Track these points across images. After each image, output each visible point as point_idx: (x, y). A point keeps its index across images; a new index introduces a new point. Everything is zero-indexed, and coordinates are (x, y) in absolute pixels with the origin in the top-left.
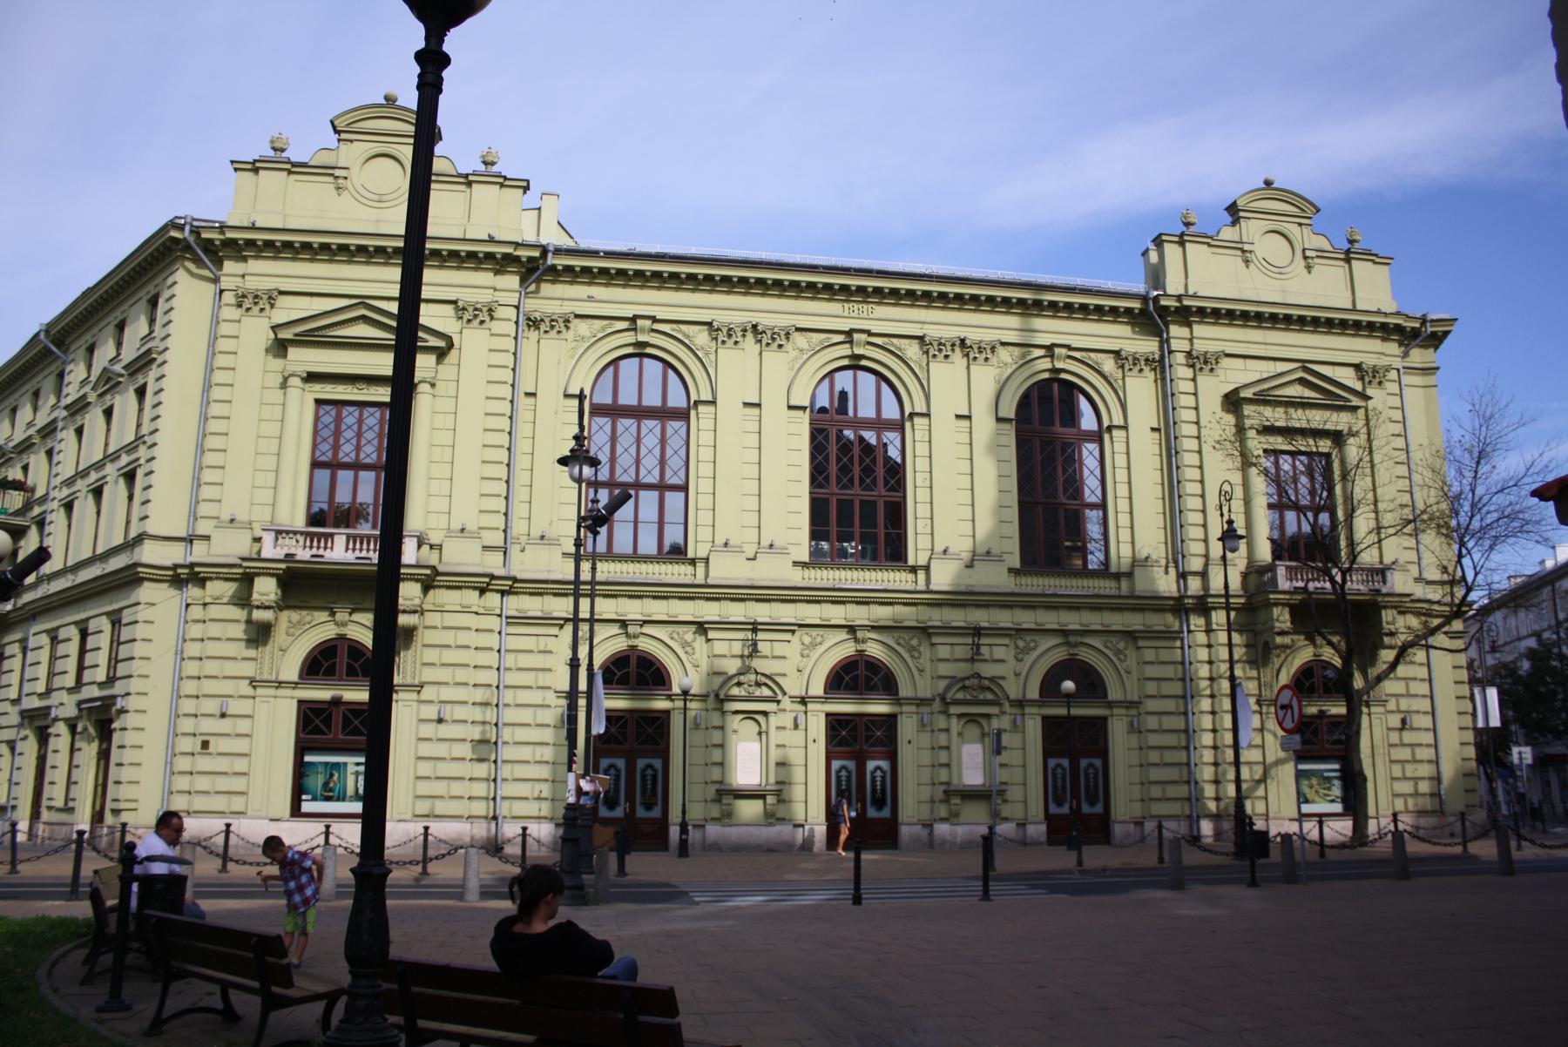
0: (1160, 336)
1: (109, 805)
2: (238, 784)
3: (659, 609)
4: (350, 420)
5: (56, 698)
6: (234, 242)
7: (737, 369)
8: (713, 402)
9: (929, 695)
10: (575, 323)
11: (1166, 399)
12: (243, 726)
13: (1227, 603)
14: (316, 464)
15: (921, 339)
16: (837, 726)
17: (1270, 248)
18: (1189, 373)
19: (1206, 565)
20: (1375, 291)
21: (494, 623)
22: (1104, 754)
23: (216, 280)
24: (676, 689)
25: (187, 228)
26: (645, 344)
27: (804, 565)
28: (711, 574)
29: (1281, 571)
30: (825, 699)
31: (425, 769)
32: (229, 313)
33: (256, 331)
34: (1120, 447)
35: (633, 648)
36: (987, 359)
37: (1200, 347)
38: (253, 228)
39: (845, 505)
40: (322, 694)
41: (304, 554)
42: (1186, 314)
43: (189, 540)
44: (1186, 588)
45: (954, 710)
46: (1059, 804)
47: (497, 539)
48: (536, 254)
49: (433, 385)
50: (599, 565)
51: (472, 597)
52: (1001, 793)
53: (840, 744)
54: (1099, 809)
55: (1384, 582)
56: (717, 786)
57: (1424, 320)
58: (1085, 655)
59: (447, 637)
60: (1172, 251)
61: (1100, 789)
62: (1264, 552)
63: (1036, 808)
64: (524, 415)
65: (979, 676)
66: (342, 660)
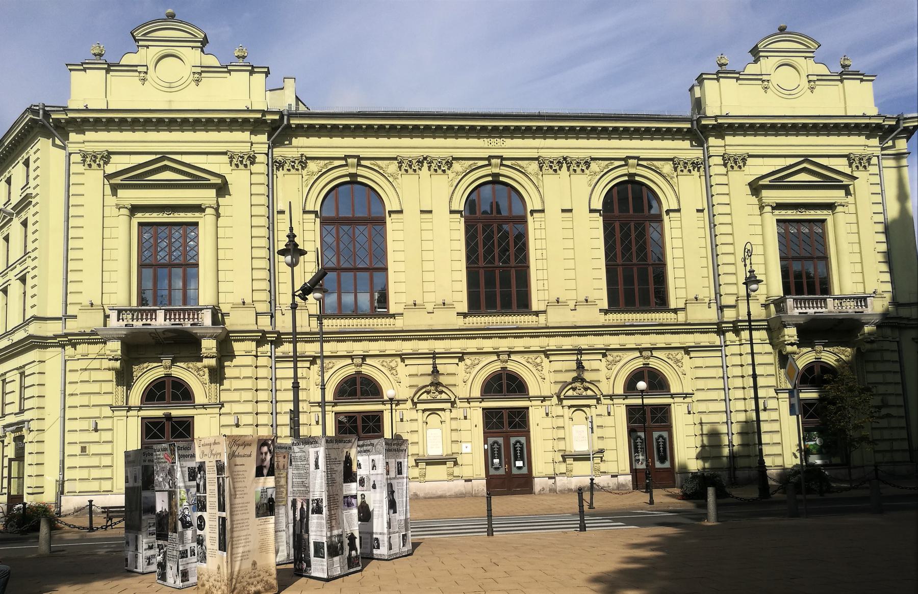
0: (702, 146)
3: (519, 344)
6: (74, 120)
8: (679, 210)
9: (549, 394)
10: (750, 161)
12: (106, 436)
13: (750, 325)
14: (141, 266)
18: (723, 170)
22: (669, 428)
23: (64, 148)
24: (386, 398)
25: (41, 112)
26: (498, 175)
29: (790, 302)
31: (106, 461)
32: (79, 168)
33: (740, 179)
35: (359, 373)
37: (731, 151)
38: (87, 110)
40: (157, 413)
41: (138, 324)
42: (721, 130)
44: (723, 317)
45: (565, 402)
47: (264, 307)
48: (277, 117)
53: (811, 416)
54: (667, 465)
55: (866, 306)
56: (562, 453)
58: (654, 363)
61: (523, 452)
62: (777, 289)
66: (168, 390)
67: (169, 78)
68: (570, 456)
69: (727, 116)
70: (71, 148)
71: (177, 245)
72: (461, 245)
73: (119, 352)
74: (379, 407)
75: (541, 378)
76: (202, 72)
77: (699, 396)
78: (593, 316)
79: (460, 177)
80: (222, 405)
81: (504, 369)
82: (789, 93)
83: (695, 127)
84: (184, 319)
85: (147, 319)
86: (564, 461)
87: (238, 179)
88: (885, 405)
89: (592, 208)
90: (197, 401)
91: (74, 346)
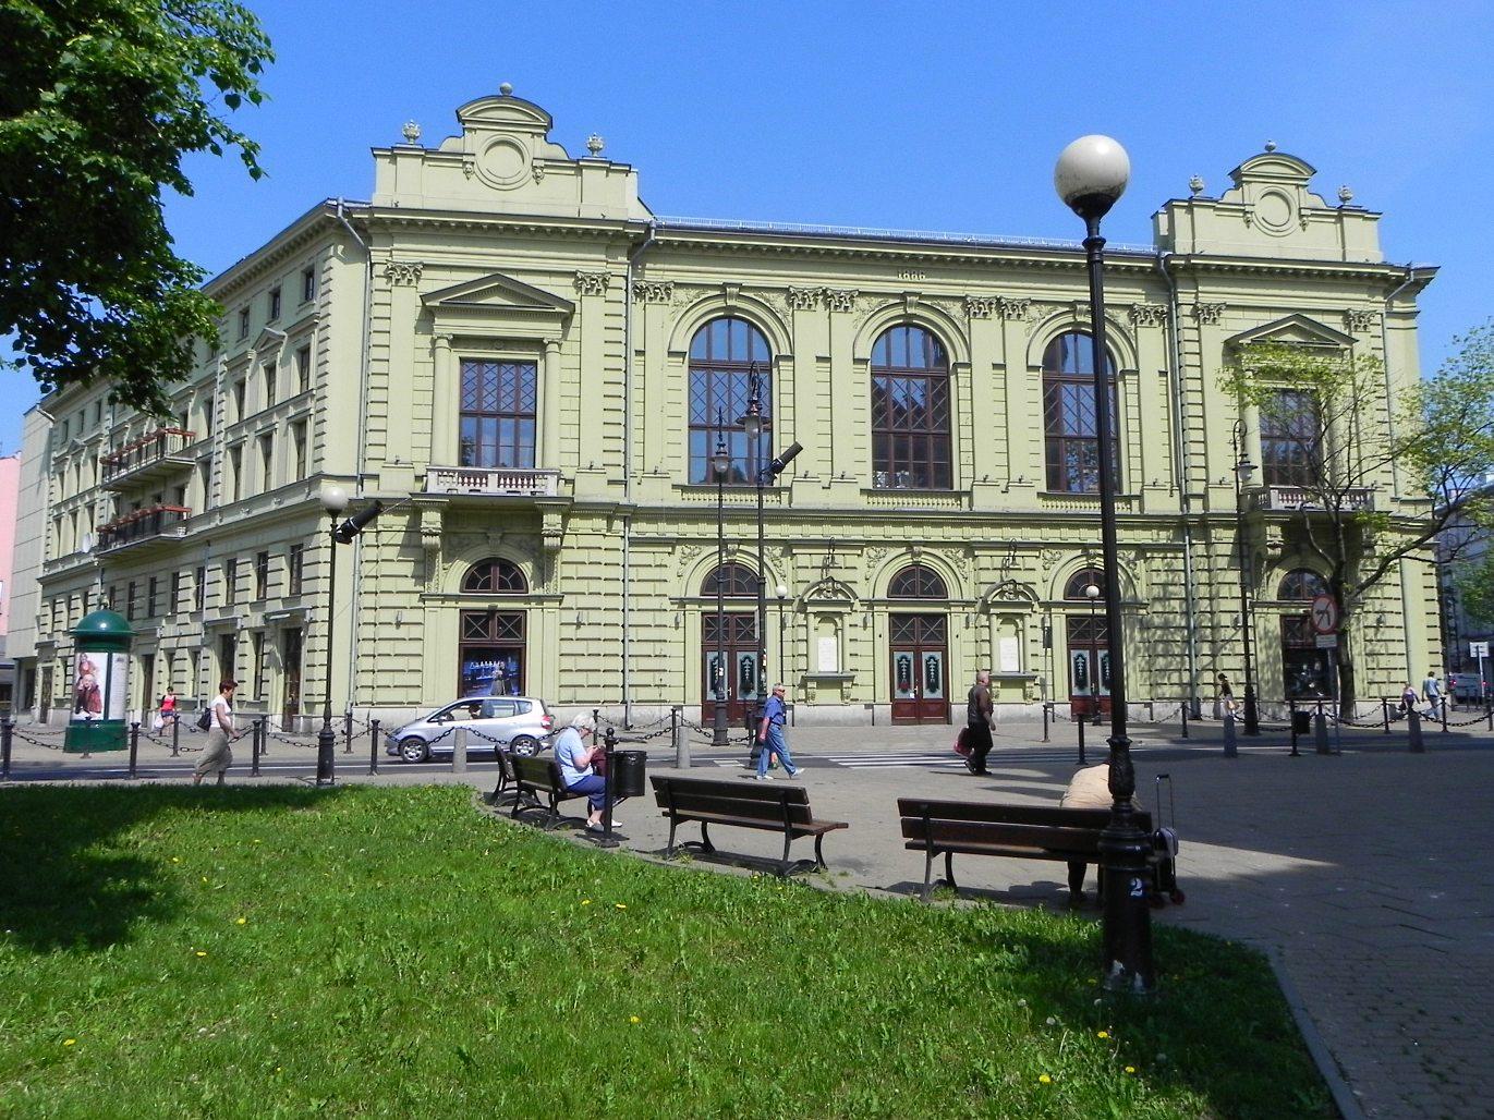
0: (1169, 290)
1: (302, 699)
2: (414, 679)
3: (935, 534)
4: (491, 376)
5: (238, 612)
7: (810, 330)
8: (969, 365)
10: (1225, 314)
11: (1173, 348)
12: (416, 632)
14: (463, 414)
15: (963, 299)
16: (709, 621)
17: (1272, 209)
18: (1189, 322)
19: (1206, 489)
20: (1364, 244)
21: (619, 543)
27: (684, 489)
28: (1212, 505)
29: (1274, 494)
30: (700, 602)
32: (381, 283)
33: (405, 303)
34: (1132, 388)
36: (1019, 315)
38: (396, 210)
39: (901, 436)
41: (464, 490)
43: (360, 479)
45: (810, 609)
46: (905, 689)
49: (560, 345)
50: (725, 496)
51: (601, 524)
52: (851, 679)
54: (939, 694)
57: (1408, 270)
59: (582, 555)
60: (1180, 214)
63: (1062, 692)
64: (636, 369)
65: (1014, 582)
67: (501, 176)
68: (812, 679)
71: (490, 388)
74: (521, 605)
75: (966, 580)
76: (546, 166)
78: (1027, 501)
79: (867, 317)
81: (916, 564)
82: (1277, 229)
84: (522, 485)
85: (475, 484)
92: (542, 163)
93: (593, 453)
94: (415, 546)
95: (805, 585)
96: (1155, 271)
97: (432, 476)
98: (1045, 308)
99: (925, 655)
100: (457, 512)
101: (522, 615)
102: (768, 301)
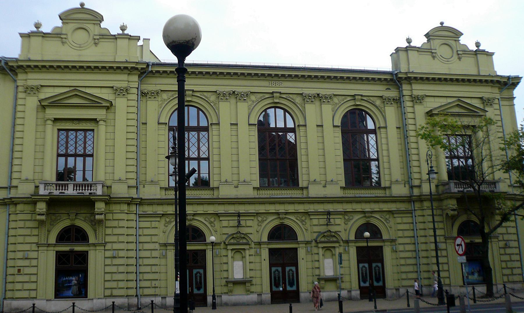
3: (291, 208)
9: (310, 240)
18: (409, 104)
19: (421, 183)
21: (133, 217)
33: (32, 102)
37: (415, 93)
40: (66, 249)
41: (56, 192)
46: (365, 282)
48: (145, 67)
52: (250, 281)
54: (381, 284)
55: (495, 187)
56: (318, 277)
58: (373, 221)
62: (445, 177)
63: (355, 284)
69: (413, 73)
70: (19, 83)
72: (255, 145)
73: (45, 210)
75: (305, 231)
76: (100, 38)
77: (400, 241)
78: (335, 191)
79: (255, 104)
80: (106, 243)
83: (395, 78)
84: (85, 190)
85: (62, 189)
86: (227, 286)
87: (120, 103)
88: (506, 246)
89: (250, 123)
90: (90, 242)
91: (16, 204)
92: (98, 37)
93: (120, 172)
94: (34, 220)
95: (226, 236)
96: (392, 80)
97: (42, 187)
98: (340, 98)
99: (287, 269)
100: (54, 203)
101: (86, 253)
102: (207, 98)
